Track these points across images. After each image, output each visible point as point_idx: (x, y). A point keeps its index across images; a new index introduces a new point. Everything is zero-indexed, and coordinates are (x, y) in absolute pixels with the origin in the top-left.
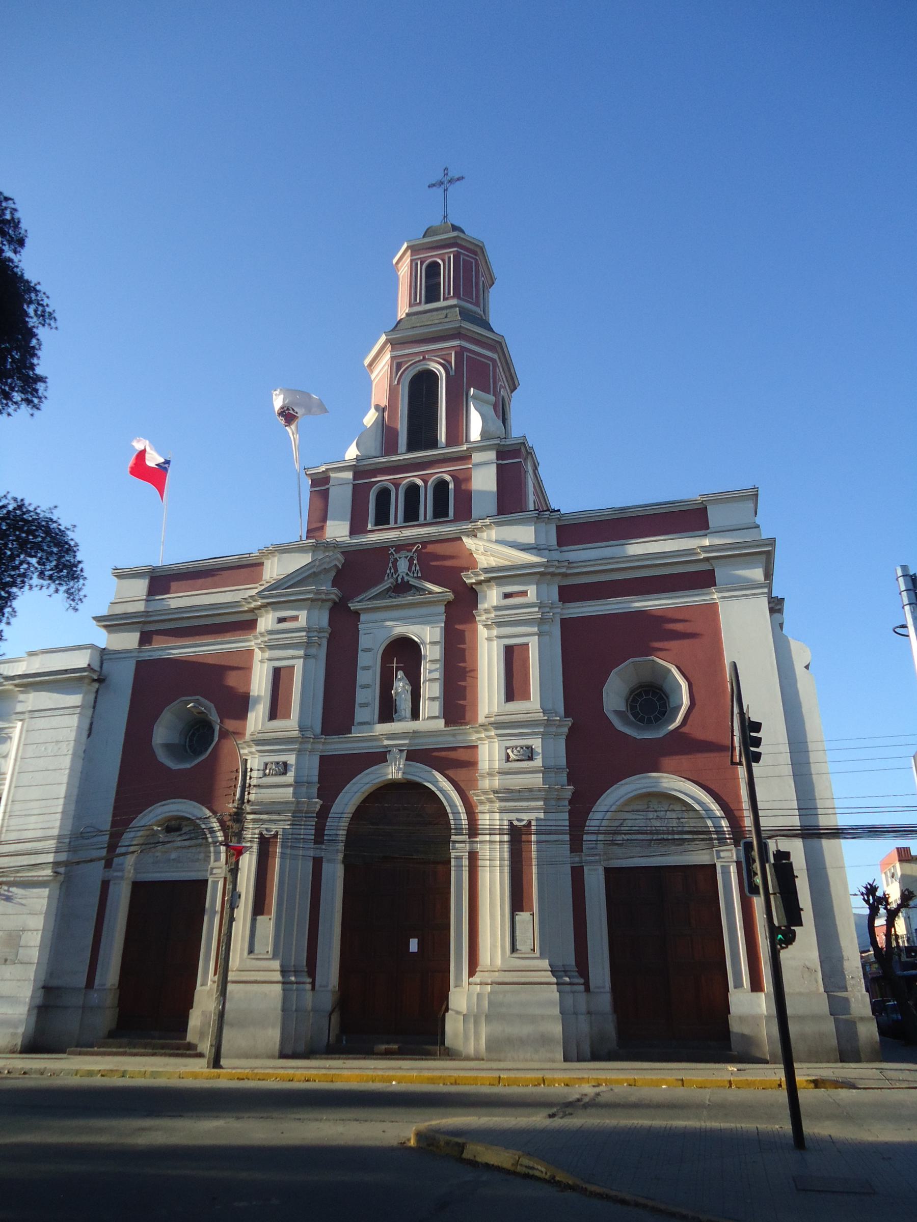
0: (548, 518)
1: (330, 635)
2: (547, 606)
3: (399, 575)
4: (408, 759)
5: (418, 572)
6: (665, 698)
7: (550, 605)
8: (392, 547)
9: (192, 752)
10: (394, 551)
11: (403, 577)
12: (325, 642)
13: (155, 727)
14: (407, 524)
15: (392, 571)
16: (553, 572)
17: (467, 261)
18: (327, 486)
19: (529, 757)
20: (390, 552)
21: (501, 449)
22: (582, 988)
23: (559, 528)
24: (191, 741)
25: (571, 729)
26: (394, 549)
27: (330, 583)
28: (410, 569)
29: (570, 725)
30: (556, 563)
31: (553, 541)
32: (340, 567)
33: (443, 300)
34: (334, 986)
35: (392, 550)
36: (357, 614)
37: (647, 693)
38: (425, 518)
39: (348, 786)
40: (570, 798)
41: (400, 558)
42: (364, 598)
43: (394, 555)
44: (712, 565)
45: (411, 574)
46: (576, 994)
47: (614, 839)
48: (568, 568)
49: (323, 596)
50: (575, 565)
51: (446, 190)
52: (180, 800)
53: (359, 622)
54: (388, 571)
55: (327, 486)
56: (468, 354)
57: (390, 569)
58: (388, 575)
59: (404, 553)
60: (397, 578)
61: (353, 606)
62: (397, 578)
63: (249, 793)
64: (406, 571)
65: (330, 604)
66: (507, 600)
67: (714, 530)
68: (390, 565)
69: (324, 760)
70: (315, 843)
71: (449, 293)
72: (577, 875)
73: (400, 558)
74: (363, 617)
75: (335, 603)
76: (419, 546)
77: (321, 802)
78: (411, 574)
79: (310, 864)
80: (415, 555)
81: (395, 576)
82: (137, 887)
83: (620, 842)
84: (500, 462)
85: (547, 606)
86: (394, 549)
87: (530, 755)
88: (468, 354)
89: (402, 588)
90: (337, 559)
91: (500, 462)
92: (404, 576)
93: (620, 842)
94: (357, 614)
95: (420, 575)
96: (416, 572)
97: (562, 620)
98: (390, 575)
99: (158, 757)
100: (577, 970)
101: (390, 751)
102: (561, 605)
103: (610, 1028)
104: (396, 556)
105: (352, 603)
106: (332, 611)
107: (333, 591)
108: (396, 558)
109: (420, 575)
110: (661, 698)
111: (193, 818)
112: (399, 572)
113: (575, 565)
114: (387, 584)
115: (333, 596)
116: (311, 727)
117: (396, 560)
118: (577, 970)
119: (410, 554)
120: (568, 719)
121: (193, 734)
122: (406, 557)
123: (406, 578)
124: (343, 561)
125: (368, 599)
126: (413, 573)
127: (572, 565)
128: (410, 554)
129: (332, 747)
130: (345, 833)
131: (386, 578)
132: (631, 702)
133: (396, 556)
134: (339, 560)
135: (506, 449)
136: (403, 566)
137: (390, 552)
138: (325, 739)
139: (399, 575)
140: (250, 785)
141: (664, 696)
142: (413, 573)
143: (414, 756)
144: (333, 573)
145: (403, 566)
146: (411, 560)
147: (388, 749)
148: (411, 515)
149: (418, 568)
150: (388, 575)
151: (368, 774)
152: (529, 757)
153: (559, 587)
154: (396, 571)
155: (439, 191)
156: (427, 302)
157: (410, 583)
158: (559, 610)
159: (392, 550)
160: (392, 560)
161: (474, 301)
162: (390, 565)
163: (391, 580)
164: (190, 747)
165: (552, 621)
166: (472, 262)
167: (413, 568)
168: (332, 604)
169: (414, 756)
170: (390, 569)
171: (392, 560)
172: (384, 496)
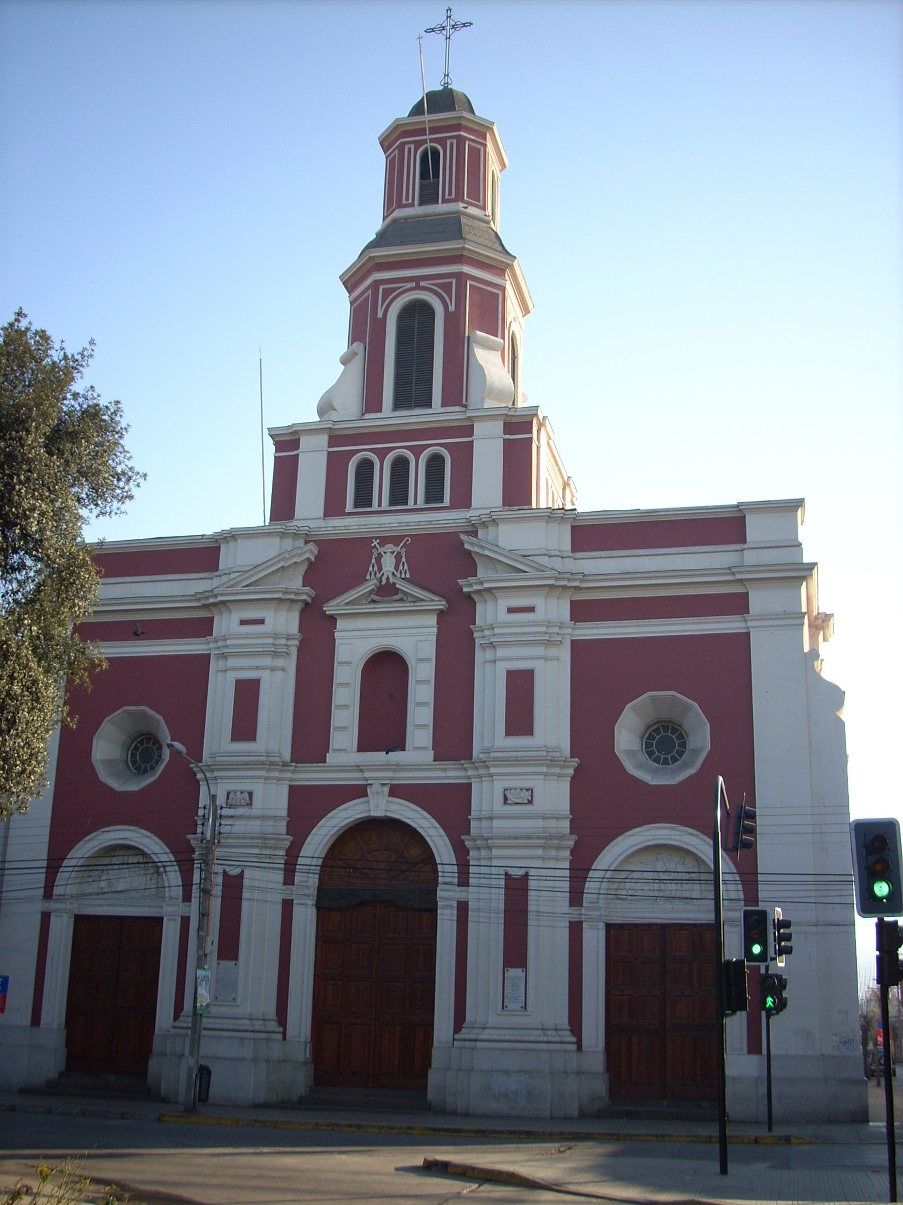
0: (562, 517)
1: (301, 642)
2: (556, 626)
3: (383, 574)
4: (391, 794)
5: (406, 571)
6: (686, 737)
7: (560, 624)
8: (376, 538)
9: (135, 769)
10: (378, 543)
11: (388, 579)
12: (294, 652)
13: (94, 740)
14: (393, 508)
15: (376, 568)
16: (564, 585)
17: (474, 147)
18: (296, 452)
19: (528, 800)
20: (373, 545)
21: (509, 420)
22: (574, 1047)
23: (573, 528)
24: (133, 756)
25: (576, 770)
26: (378, 541)
27: (300, 580)
28: (396, 568)
29: (576, 765)
30: (569, 576)
31: (567, 545)
32: (313, 560)
33: (442, 203)
34: (307, 1038)
35: (375, 543)
36: (333, 619)
37: (666, 728)
38: (415, 503)
39: (324, 820)
40: (572, 847)
41: (385, 553)
42: (340, 602)
43: (377, 549)
44: (746, 587)
45: (398, 575)
46: (565, 559)
47: (618, 893)
48: (582, 581)
49: (292, 596)
50: (590, 578)
51: (448, 38)
52: (126, 827)
53: (336, 629)
54: (371, 569)
55: (296, 452)
56: (473, 283)
57: (373, 566)
58: (371, 573)
59: (389, 547)
60: (381, 578)
61: (330, 608)
62: (381, 578)
63: (220, 825)
64: (392, 569)
65: (299, 606)
66: (423, 207)
67: (752, 546)
68: (373, 561)
69: (294, 790)
70: (459, 885)
71: (450, 194)
72: (576, 929)
73: (385, 553)
74: (340, 624)
75: (307, 604)
76: (408, 540)
77: (291, 838)
78: (398, 575)
79: (279, 908)
80: (403, 551)
81: (378, 576)
82: (81, 921)
83: (624, 897)
84: (508, 437)
85: (556, 626)
86: (378, 541)
87: (530, 799)
88: (473, 283)
89: (387, 591)
90: (310, 551)
91: (508, 437)
92: (390, 576)
93: (624, 897)
94: (333, 619)
95: (408, 576)
96: (403, 572)
97: (573, 642)
98: (373, 573)
99: (100, 776)
100: (569, 1028)
101: (371, 784)
102: (572, 625)
103: (600, 1087)
104: (381, 550)
105: (327, 607)
106: (302, 613)
107: (305, 591)
108: (380, 553)
109: (408, 576)
110: (681, 737)
111: (149, 852)
112: (384, 570)
113: (590, 578)
114: (370, 585)
115: (304, 597)
116: (279, 752)
117: (380, 556)
118: (569, 1028)
119: (398, 549)
120: (574, 759)
121: (136, 748)
122: (393, 553)
123: (391, 580)
124: (316, 552)
125: (348, 604)
126: (401, 573)
127: (586, 578)
128: (398, 549)
129: (302, 776)
130: (45, 865)
131: (368, 577)
132: (647, 739)
133: (381, 550)
134: (310, 552)
135: (515, 420)
136: (388, 563)
137: (373, 545)
138: (296, 767)
139: (383, 574)
140: (221, 816)
141: (683, 733)
142: (401, 573)
143: (396, 791)
144: (304, 568)
145: (388, 563)
146: (398, 557)
147: (370, 782)
148: (399, 495)
149: (406, 567)
150: (371, 573)
151: (344, 810)
152: (528, 800)
153: (571, 601)
154: (380, 569)
155: (440, 38)
156: (422, 203)
157: (397, 586)
158: (570, 631)
159: (375, 543)
160: (375, 555)
161: (481, 204)
162: (373, 561)
163: (375, 581)
164: (134, 763)
165: (561, 643)
166: (479, 150)
167: (401, 567)
168: (303, 605)
169: (396, 791)
170: (373, 566)
171: (375, 555)
172: (365, 470)
